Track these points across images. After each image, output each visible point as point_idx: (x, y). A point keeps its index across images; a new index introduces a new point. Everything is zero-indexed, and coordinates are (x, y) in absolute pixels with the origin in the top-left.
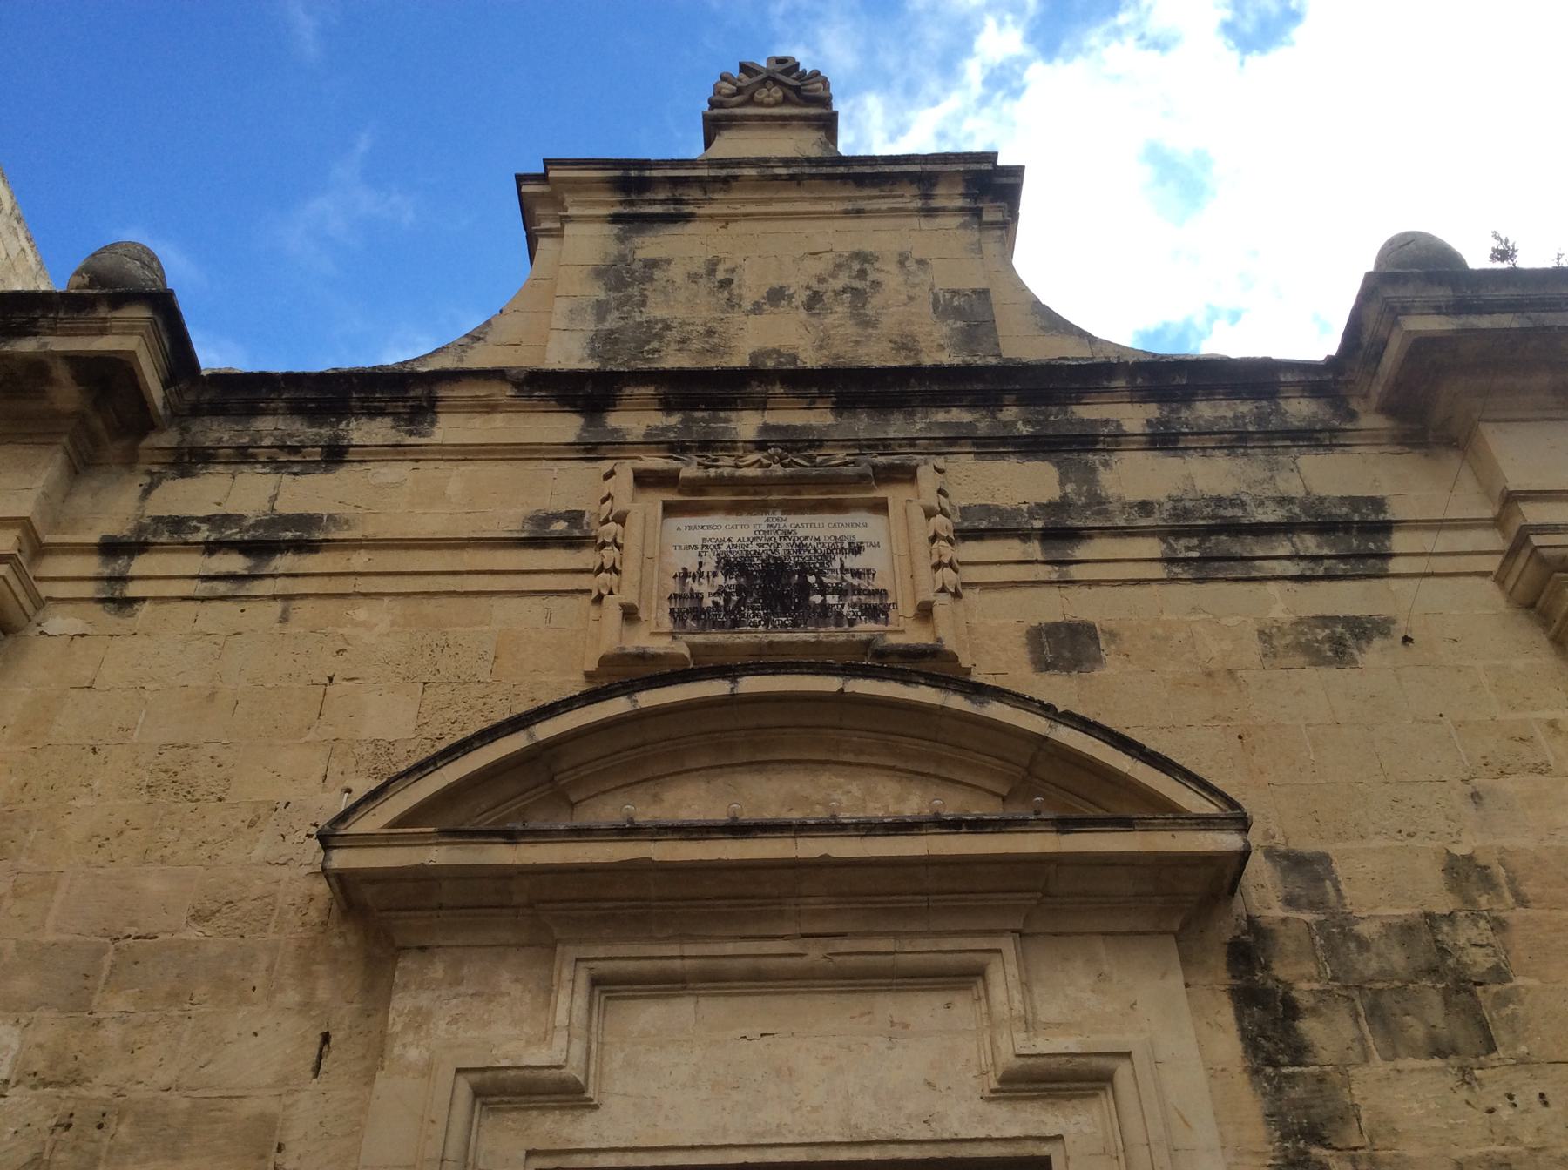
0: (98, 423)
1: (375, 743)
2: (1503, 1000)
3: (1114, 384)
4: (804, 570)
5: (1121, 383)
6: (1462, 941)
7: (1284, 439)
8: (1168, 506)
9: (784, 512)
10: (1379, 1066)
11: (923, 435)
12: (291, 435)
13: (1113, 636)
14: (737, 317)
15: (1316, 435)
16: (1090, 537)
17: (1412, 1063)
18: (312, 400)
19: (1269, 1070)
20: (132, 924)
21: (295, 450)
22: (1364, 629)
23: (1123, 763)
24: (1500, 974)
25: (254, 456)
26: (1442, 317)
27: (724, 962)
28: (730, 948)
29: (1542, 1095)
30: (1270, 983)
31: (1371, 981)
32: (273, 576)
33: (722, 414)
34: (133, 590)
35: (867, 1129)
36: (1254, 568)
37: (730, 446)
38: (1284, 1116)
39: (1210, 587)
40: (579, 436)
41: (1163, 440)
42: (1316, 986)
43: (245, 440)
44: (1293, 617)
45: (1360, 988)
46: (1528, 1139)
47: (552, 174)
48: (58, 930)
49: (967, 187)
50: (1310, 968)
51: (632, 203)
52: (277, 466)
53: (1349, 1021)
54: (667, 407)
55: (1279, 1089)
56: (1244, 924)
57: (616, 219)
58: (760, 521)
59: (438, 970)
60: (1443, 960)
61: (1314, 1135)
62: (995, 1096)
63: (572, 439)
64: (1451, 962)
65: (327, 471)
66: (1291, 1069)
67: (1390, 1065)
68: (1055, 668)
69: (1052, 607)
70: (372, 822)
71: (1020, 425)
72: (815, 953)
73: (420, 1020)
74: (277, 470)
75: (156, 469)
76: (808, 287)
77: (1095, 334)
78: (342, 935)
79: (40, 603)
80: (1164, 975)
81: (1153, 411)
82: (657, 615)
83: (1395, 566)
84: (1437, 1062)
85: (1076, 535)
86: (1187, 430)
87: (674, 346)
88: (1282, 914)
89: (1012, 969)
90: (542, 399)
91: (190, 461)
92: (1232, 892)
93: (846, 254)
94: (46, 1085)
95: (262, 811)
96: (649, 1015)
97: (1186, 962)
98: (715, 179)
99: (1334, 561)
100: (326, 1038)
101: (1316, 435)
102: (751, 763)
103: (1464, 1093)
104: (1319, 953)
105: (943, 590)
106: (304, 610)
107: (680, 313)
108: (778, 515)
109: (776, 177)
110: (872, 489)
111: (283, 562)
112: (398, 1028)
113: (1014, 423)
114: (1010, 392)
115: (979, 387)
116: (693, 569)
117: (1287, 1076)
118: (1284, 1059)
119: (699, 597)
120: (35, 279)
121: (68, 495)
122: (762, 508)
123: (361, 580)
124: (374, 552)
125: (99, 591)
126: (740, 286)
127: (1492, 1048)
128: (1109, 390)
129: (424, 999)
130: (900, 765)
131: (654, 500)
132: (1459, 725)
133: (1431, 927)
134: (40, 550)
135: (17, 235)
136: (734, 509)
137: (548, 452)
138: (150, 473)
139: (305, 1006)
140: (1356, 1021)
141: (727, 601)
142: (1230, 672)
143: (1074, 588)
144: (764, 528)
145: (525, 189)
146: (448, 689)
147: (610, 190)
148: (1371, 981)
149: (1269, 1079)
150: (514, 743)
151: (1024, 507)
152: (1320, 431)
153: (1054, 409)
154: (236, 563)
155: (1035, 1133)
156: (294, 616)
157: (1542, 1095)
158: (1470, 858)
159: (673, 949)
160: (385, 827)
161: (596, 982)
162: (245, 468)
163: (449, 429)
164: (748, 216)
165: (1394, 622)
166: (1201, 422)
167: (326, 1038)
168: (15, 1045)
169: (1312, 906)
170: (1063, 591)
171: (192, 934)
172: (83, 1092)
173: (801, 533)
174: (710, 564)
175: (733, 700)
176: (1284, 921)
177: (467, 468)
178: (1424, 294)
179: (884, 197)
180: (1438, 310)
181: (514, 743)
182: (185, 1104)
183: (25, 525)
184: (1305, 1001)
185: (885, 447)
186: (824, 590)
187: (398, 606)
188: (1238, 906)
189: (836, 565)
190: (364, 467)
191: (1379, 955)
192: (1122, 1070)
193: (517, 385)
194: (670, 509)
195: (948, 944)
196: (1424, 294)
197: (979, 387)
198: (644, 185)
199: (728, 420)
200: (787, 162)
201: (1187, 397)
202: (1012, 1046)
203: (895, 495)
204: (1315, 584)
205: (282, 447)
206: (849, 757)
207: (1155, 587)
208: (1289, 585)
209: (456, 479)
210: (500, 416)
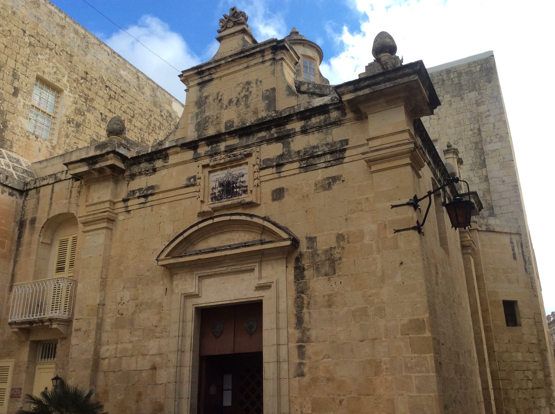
2: (339, 264)
3: (294, 118)
4: (234, 183)
5: (295, 118)
6: (335, 253)
7: (330, 125)
8: (303, 151)
9: (231, 168)
10: (315, 279)
11: (255, 142)
12: (147, 167)
13: (287, 189)
14: (223, 111)
15: (337, 123)
16: (285, 164)
17: (321, 278)
18: (148, 159)
19: (297, 281)
20: (140, 273)
21: (148, 171)
22: (335, 179)
24: (340, 259)
25: (142, 173)
26: (352, 93)
27: (217, 272)
28: (217, 270)
29: (341, 282)
30: (301, 265)
31: (318, 262)
32: (149, 202)
34: (130, 209)
36: (317, 167)
38: (298, 289)
39: (308, 173)
40: (193, 157)
41: (304, 131)
42: (308, 265)
43: (140, 170)
44: (322, 179)
45: (316, 264)
46: (336, 290)
48: (131, 275)
49: (272, 50)
50: (308, 261)
51: (201, 78)
52: (146, 175)
53: (312, 271)
54: (208, 145)
55: (298, 285)
56: (299, 253)
58: (226, 171)
59: (179, 277)
60: (331, 257)
61: (302, 292)
62: (255, 290)
63: (192, 158)
64: (332, 257)
65: (154, 174)
66: (301, 281)
67: (317, 279)
68: (276, 200)
69: (277, 184)
70: (162, 257)
71: (275, 135)
72: (229, 269)
73: (177, 285)
74: (146, 176)
75: (128, 179)
76: (237, 97)
78: (167, 272)
79: (117, 214)
80: (282, 266)
81: (302, 123)
82: (208, 201)
83: (345, 160)
84: (325, 277)
85: (282, 165)
86: (309, 128)
87: (211, 124)
88: (306, 251)
90: (185, 149)
91: (133, 177)
93: (245, 83)
94: (134, 300)
96: (207, 281)
97: (287, 263)
98: (216, 66)
99: (333, 161)
100: (166, 289)
101: (337, 123)
102: (221, 233)
103: (328, 283)
104: (310, 258)
106: (155, 208)
107: (212, 113)
109: (229, 62)
110: (245, 160)
111: (150, 198)
113: (274, 134)
114: (272, 125)
115: (266, 126)
116: (214, 187)
117: (300, 282)
118: (300, 279)
119: (215, 193)
120: (124, 65)
121: (116, 188)
122: (226, 168)
124: (163, 193)
125: (125, 210)
126: (223, 101)
127: (335, 274)
128: (293, 120)
131: (207, 170)
133: (331, 250)
134: (114, 203)
135: (115, 57)
136: (222, 169)
137: (189, 161)
138: (127, 180)
139: (164, 284)
140: (314, 271)
141: (220, 194)
143: (282, 178)
146: (177, 222)
148: (318, 262)
149: (297, 283)
150: (181, 238)
151: (275, 157)
152: (338, 121)
153: (282, 127)
154: (142, 200)
155: (260, 296)
156: (154, 210)
157: (341, 282)
158: (342, 234)
159: (209, 271)
162: (141, 176)
163: (172, 159)
164: (225, 75)
165: (342, 176)
166: (312, 125)
167: (166, 289)
168: (129, 294)
169: (311, 248)
170: (280, 179)
171: (148, 274)
172: (138, 301)
173: (233, 173)
174: (217, 184)
175: (213, 223)
177: (176, 168)
178: (347, 89)
179: (254, 59)
180: (351, 92)
181: (181, 238)
182: (151, 301)
183: (110, 201)
184: (306, 267)
185: (249, 146)
186: (237, 187)
188: (299, 250)
189: (239, 181)
190: (160, 172)
191: (320, 257)
193: (180, 147)
194: (210, 172)
195: (249, 265)
196: (347, 89)
197: (266, 126)
199: (219, 146)
200: (230, 56)
201: (310, 118)
202: (256, 282)
204: (329, 168)
205: (146, 171)
206: (236, 229)
207: (297, 175)
208: (323, 169)
210: (179, 154)
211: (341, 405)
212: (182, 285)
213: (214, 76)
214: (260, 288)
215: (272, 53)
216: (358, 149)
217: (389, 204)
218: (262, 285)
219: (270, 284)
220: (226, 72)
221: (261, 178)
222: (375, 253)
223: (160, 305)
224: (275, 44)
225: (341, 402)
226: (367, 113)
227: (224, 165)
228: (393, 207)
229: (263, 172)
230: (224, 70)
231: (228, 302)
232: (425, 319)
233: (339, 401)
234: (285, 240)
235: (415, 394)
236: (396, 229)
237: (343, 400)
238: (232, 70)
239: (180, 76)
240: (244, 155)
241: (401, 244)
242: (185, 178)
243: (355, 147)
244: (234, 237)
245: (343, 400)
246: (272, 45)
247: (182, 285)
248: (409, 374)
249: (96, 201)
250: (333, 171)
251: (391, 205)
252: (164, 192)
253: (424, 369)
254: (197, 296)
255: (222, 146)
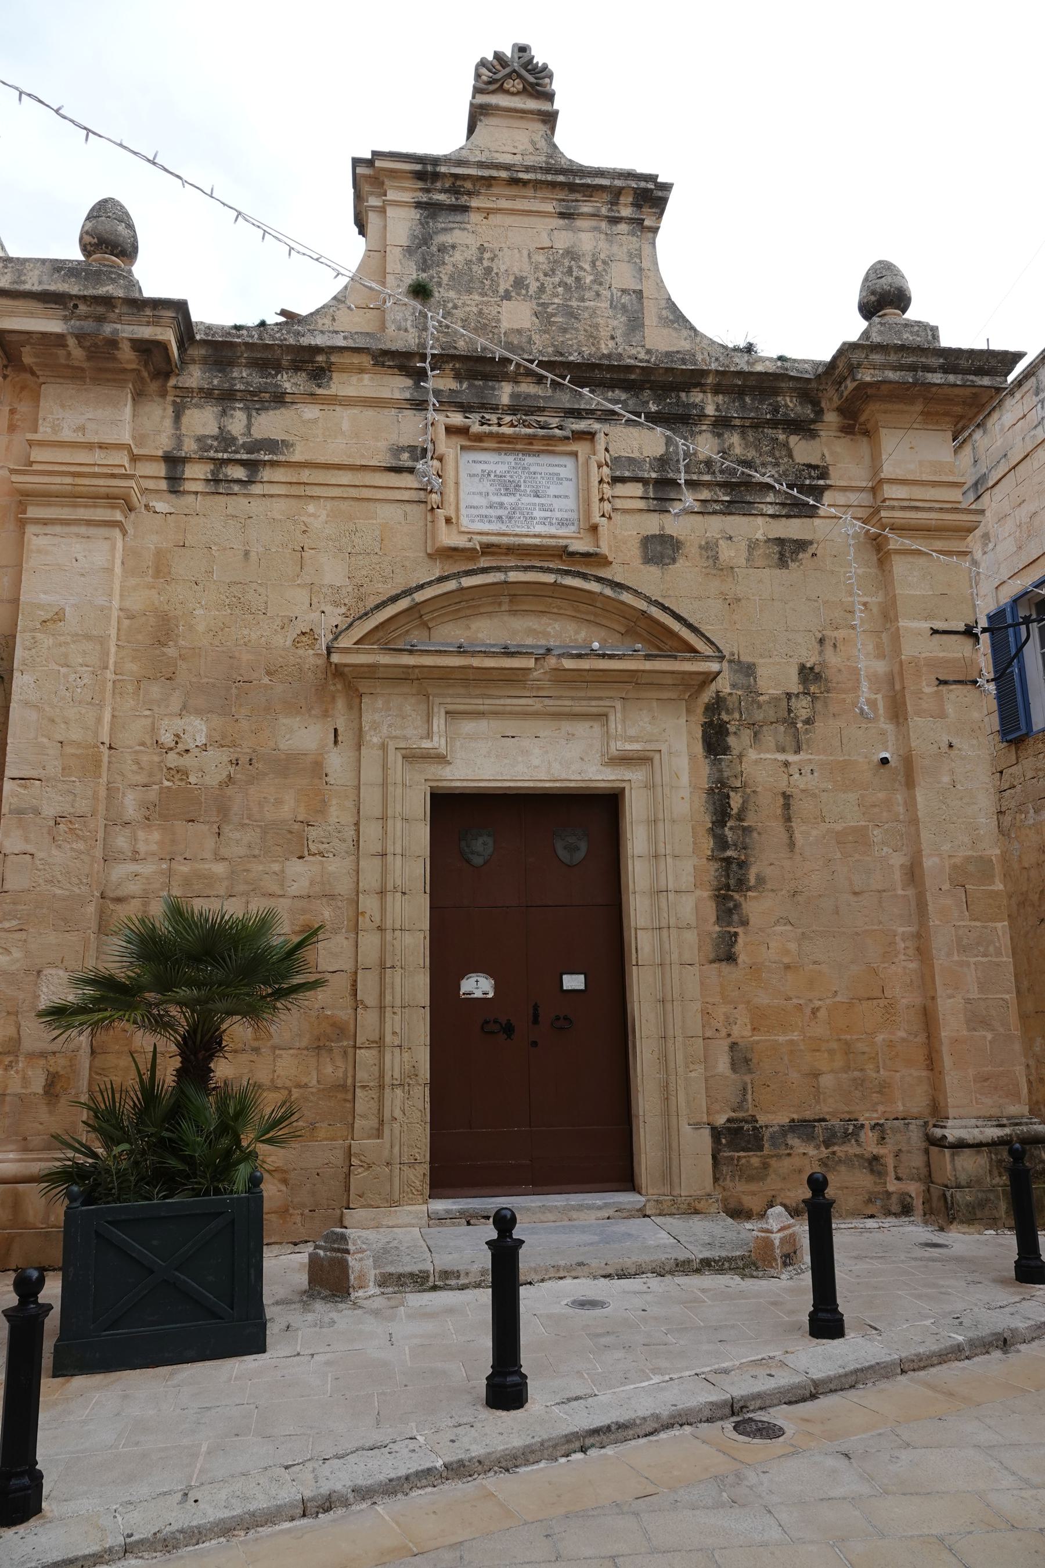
0: (145, 374)
1: (331, 586)
23: (675, 626)
33: (490, 383)
35: (556, 776)
36: (753, 508)
37: (494, 408)
47: (378, 164)
54: (458, 377)
57: (418, 205)
59: (380, 703)
77: (699, 328)
89: (619, 715)
90: (390, 367)
92: (712, 681)
93: (561, 252)
95: (286, 621)
96: (468, 726)
97: (689, 711)
100: (336, 730)
105: (603, 516)
108: (520, 456)
112: (367, 728)
123: (307, 488)
129: (377, 717)
130: (578, 615)
132: (825, 602)
142: (732, 568)
144: (513, 464)
145: (359, 170)
147: (413, 178)
160: (355, 644)
161: (447, 713)
163: (342, 385)
164: (499, 210)
170: (662, 516)
176: (730, 694)
187: (329, 504)
192: (657, 756)
193: (374, 357)
198: (436, 176)
203: (581, 448)
206: (555, 610)
208: (768, 519)
209: (345, 417)
211: (816, 1017)
212: (390, 726)
213: (474, 203)
214: (625, 760)
215: (633, 205)
216: (849, 494)
217: (926, 625)
218: (631, 753)
219: (651, 754)
220: (504, 204)
221: (617, 500)
222: (882, 719)
223: (317, 769)
224: (651, 186)
225: (814, 1011)
226: (880, 424)
227: (509, 443)
228: (935, 632)
229: (621, 489)
230: (498, 197)
231: (531, 784)
232: (993, 858)
233: (810, 1009)
234: (707, 658)
235: (974, 994)
236: (941, 678)
237: (818, 1009)
238: (520, 205)
239: (356, 162)
240: (573, 432)
241: (950, 709)
242: (382, 445)
243: (845, 489)
244: (549, 629)
245: (818, 1009)
246: (643, 184)
247: (390, 726)
248: (965, 959)
249: (67, 435)
250: (794, 529)
251: (932, 629)
252: (316, 467)
253: (991, 949)
254: (441, 759)
255: (505, 393)
